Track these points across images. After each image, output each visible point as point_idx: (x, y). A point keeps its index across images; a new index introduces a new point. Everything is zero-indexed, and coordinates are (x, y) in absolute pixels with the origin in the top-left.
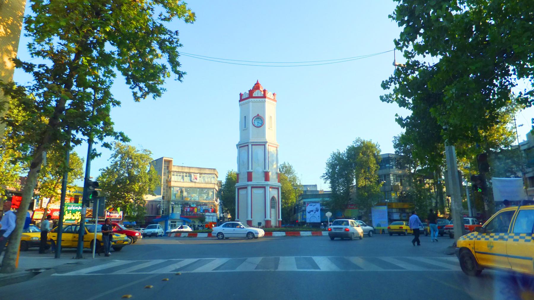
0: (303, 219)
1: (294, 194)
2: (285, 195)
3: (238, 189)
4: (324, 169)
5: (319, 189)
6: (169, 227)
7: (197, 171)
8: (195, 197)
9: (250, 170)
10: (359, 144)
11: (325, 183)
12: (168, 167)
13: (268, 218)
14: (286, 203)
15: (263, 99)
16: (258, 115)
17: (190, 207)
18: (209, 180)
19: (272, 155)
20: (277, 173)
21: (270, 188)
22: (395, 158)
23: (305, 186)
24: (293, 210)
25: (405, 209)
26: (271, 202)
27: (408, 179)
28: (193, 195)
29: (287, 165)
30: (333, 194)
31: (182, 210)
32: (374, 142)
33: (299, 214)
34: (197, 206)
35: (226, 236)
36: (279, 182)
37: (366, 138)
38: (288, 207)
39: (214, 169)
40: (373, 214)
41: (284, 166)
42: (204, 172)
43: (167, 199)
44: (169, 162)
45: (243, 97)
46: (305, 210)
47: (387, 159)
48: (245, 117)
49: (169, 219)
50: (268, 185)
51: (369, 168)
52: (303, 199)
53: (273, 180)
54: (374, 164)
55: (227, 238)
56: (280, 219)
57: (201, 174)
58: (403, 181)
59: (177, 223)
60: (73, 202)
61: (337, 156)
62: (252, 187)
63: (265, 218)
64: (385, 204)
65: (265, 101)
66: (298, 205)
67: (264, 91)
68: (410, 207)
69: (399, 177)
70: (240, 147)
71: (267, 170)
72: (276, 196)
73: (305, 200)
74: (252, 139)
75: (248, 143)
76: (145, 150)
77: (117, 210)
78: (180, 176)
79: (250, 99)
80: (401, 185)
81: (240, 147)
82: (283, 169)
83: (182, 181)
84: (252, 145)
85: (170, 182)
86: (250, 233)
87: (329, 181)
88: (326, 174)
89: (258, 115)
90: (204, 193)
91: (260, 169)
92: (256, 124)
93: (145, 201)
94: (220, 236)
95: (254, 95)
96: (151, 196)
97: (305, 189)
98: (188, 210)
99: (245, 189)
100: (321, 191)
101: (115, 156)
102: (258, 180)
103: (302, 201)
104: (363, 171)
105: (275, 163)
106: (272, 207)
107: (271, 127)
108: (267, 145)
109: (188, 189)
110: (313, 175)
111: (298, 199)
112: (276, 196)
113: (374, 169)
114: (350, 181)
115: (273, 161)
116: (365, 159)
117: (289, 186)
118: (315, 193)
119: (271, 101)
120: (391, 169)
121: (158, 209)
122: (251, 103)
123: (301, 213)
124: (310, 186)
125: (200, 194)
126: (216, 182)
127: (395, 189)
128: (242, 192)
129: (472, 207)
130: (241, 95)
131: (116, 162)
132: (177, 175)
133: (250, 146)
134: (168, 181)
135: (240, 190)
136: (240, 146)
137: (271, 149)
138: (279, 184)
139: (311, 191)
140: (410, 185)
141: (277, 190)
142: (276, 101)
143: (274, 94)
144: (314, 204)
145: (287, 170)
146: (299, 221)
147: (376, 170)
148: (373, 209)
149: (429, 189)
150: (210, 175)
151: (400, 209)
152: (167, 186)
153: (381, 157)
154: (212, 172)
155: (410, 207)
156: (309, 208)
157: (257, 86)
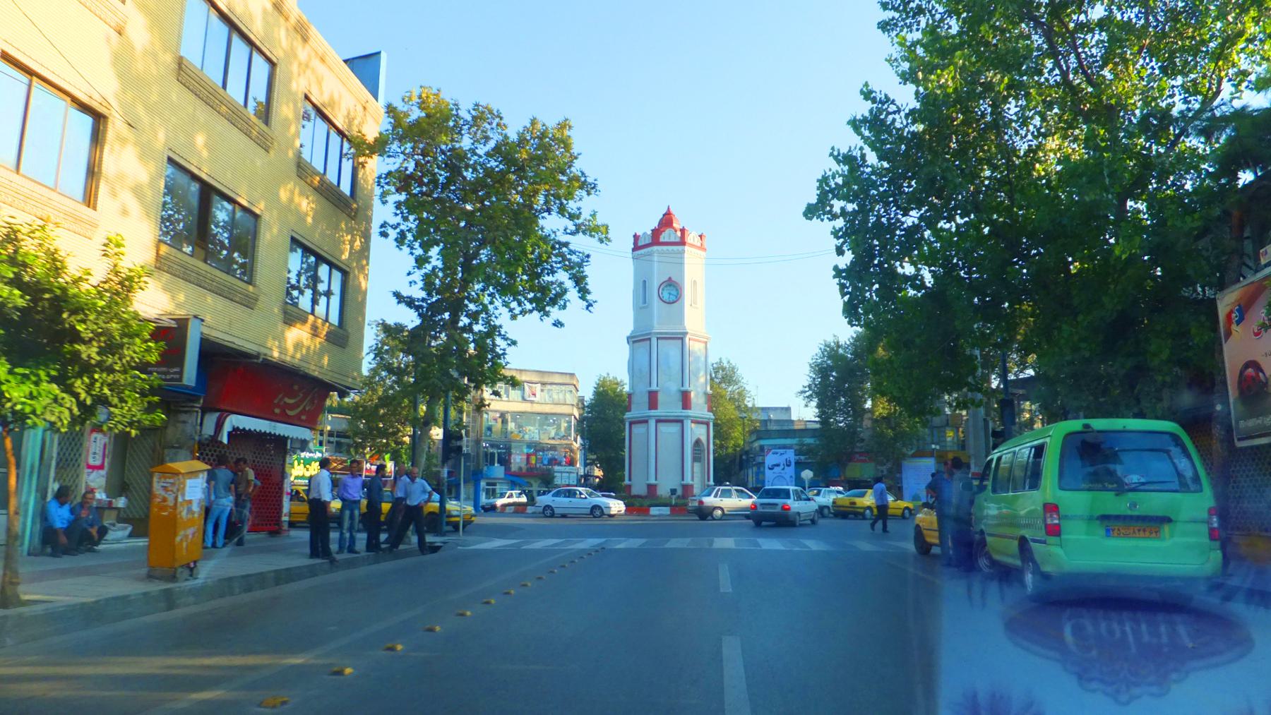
0: (757, 480)
1: (740, 428)
2: (721, 431)
3: (631, 424)
4: (803, 376)
5: (794, 417)
7: (535, 378)
9: (654, 388)
13: (688, 480)
14: (721, 447)
15: (680, 248)
18: (561, 396)
19: (698, 358)
20: (706, 394)
23: (763, 409)
29: (725, 364)
30: (825, 428)
34: (537, 451)
35: (556, 511)
38: (727, 455)
39: (572, 375)
40: (904, 476)
45: (640, 244)
50: (688, 417)
52: (759, 438)
53: (699, 407)
55: (564, 516)
57: (543, 384)
59: (498, 487)
61: (832, 349)
62: (658, 421)
64: (931, 454)
66: (747, 453)
67: (683, 231)
71: (686, 388)
72: (704, 439)
73: (762, 442)
79: (655, 248)
86: (595, 507)
87: (814, 403)
88: (809, 386)
91: (674, 387)
92: (666, 296)
94: (548, 512)
95: (662, 240)
97: (763, 417)
99: (644, 425)
103: (756, 445)
106: (696, 459)
108: (687, 339)
109: (518, 415)
111: (748, 439)
112: (704, 439)
115: (698, 370)
117: (730, 411)
123: (755, 469)
128: (638, 430)
130: (636, 237)
133: (654, 340)
136: (634, 340)
137: (694, 346)
138: (711, 415)
139: (777, 422)
141: (705, 427)
143: (701, 236)
145: (724, 376)
150: (563, 388)
154: (567, 380)
156: (770, 459)
157: (667, 221)
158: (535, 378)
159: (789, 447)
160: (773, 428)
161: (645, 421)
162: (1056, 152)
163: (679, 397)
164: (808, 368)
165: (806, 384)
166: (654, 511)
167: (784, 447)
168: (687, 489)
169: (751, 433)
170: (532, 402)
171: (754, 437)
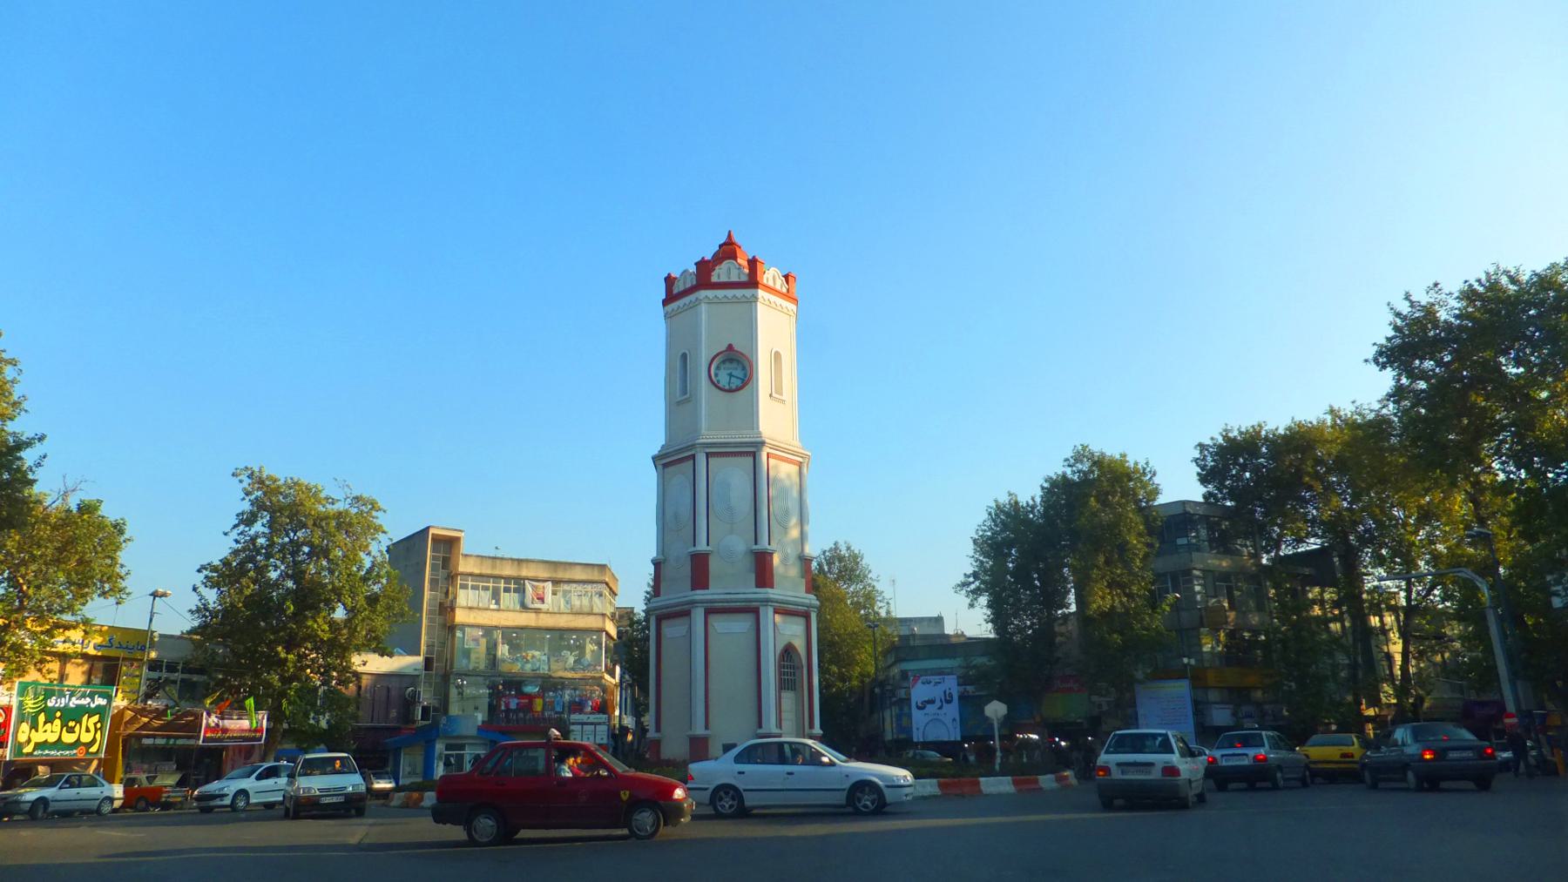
2: (833, 649)
4: (963, 560)
7: (543, 573)
8: (537, 659)
9: (702, 546)
10: (1085, 467)
11: (971, 606)
15: (748, 292)
16: (730, 347)
17: (521, 694)
18: (585, 601)
19: (784, 492)
21: (776, 612)
22: (1207, 517)
24: (867, 699)
26: (781, 667)
27: (1253, 587)
28: (530, 653)
29: (844, 552)
31: (490, 705)
32: (1135, 458)
33: (887, 714)
34: (544, 689)
36: (808, 591)
37: (1109, 446)
38: (851, 690)
39: (602, 567)
41: (834, 557)
42: (567, 575)
43: (440, 669)
44: (448, 545)
46: (909, 700)
47: (1181, 518)
48: (684, 356)
50: (767, 601)
51: (1123, 548)
52: (899, 660)
54: (1140, 535)
58: (1237, 593)
60: (95, 680)
62: (709, 612)
63: (760, 726)
64: (1180, 674)
65: (756, 298)
66: (882, 684)
67: (753, 263)
69: (1220, 581)
71: (764, 544)
72: (800, 644)
75: (693, 446)
76: (357, 499)
77: (243, 708)
78: (486, 589)
79: (703, 294)
80: (1232, 607)
81: (665, 466)
82: (830, 564)
83: (493, 606)
84: (708, 455)
85: (453, 609)
87: (983, 600)
88: (975, 575)
89: (730, 347)
90: (569, 648)
91: (739, 544)
92: (724, 380)
93: (357, 675)
95: (714, 279)
96: (376, 656)
97: (904, 631)
98: (513, 706)
99: (684, 620)
100: (957, 635)
101: (248, 520)
102: (729, 582)
103: (895, 671)
104: (1101, 559)
105: (794, 520)
106: (787, 682)
107: (779, 391)
110: (930, 582)
111: (881, 664)
112: (800, 644)
113: (1141, 550)
114: (1054, 598)
115: (787, 513)
116: (1106, 517)
118: (938, 642)
119: (779, 301)
120: (1195, 555)
121: (409, 703)
122: (704, 307)
123: (895, 710)
124: (922, 620)
126: (609, 610)
127: (1213, 620)
129: (1514, 676)
130: (669, 281)
131: (253, 539)
132: (474, 588)
134: (446, 608)
135: (664, 624)
136: (665, 461)
138: (812, 599)
140: (1260, 608)
141: (802, 621)
142: (795, 301)
143: (786, 277)
144: (937, 678)
145: (845, 566)
146: (888, 737)
147: (1146, 556)
149: (1324, 621)
150: (589, 587)
152: (444, 626)
156: (919, 692)
157: (728, 250)
158: (543, 573)
160: (925, 645)
161: (683, 613)
164: (972, 546)
165: (970, 571)
167: (940, 672)
169: (885, 653)
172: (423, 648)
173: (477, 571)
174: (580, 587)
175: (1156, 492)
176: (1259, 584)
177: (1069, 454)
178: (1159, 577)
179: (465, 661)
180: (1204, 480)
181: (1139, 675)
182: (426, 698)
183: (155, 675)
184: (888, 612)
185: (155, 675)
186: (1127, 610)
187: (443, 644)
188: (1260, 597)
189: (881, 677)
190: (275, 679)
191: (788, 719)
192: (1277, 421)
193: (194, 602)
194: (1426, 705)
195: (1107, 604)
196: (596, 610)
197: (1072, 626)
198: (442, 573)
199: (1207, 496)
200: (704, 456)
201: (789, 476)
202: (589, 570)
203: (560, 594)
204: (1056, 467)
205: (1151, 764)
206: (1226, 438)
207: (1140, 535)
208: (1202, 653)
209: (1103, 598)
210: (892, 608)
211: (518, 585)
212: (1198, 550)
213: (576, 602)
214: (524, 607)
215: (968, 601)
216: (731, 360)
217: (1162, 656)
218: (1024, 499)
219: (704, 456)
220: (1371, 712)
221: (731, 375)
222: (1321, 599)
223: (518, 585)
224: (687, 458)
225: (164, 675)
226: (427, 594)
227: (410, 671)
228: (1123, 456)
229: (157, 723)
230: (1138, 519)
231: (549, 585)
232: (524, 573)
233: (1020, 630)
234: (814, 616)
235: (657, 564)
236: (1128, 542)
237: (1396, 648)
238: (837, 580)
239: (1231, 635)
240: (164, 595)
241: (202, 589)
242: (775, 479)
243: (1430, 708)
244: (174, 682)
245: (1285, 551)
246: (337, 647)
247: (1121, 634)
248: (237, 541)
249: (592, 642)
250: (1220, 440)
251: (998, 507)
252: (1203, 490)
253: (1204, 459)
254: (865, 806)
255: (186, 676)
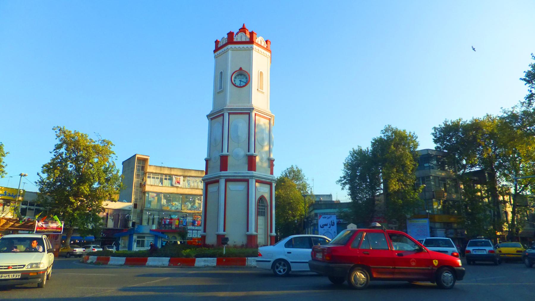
4: (340, 172)
6: (135, 245)
7: (180, 173)
8: (176, 205)
9: (225, 152)
10: (389, 134)
11: (343, 189)
12: (143, 168)
13: (252, 231)
15: (249, 46)
16: (241, 69)
19: (262, 130)
21: (257, 181)
23: (317, 196)
25: (451, 223)
28: (174, 203)
29: (295, 169)
42: (189, 174)
44: (144, 161)
47: (426, 157)
48: (221, 73)
49: (134, 233)
50: (252, 177)
51: (404, 166)
52: (314, 209)
56: (274, 234)
58: (448, 186)
59: (146, 239)
62: (227, 181)
63: (248, 231)
64: (426, 216)
65: (252, 48)
66: (307, 218)
67: (252, 34)
68: (459, 220)
70: (212, 119)
71: (252, 152)
72: (267, 196)
73: (316, 211)
74: (230, 103)
76: (104, 141)
78: (158, 178)
79: (230, 46)
81: (212, 119)
84: (229, 114)
85: (145, 185)
87: (347, 186)
88: (344, 177)
89: (241, 69)
91: (242, 152)
92: (238, 83)
95: (235, 40)
97: (317, 199)
101: (59, 147)
104: (395, 170)
105: (266, 143)
106: (260, 212)
107: (262, 88)
110: (327, 181)
111: (307, 211)
112: (267, 196)
114: (373, 187)
115: (263, 140)
119: (263, 51)
120: (432, 170)
121: (126, 220)
122: (230, 52)
123: (312, 228)
125: (183, 202)
130: (217, 42)
132: (153, 178)
133: (226, 115)
134: (142, 185)
136: (213, 117)
140: (457, 192)
141: (268, 186)
142: (270, 51)
143: (267, 41)
144: (329, 216)
145: (295, 174)
148: (409, 222)
149: (482, 198)
150: (197, 179)
151: (444, 223)
153: (420, 154)
155: (459, 220)
156: (322, 221)
158: (180, 173)
159: (334, 214)
160: (326, 204)
162: (387, 164)
163: (245, 160)
164: (343, 166)
165: (342, 176)
166: (200, 262)
168: (251, 239)
169: (309, 207)
170: (177, 187)
171: (311, 209)
172: (133, 199)
173: (154, 172)
174: (193, 179)
175: (416, 145)
176: (456, 182)
177: (383, 128)
178: (417, 179)
179: (149, 205)
180: (436, 141)
181: (408, 216)
182: (133, 218)
183: (24, 207)
184: (311, 192)
185: (24, 207)
186: (405, 190)
187: (141, 198)
188: (457, 187)
189: (307, 215)
190: (69, 210)
191: (260, 228)
192: (467, 118)
193: (38, 178)
194: (520, 232)
195: (397, 188)
196: (199, 188)
197: (382, 197)
198: (141, 172)
199: (437, 148)
200: (228, 115)
201: (265, 124)
202: (197, 172)
203: (186, 181)
204: (378, 134)
205: (447, 252)
206: (446, 125)
207: (411, 161)
208: (433, 208)
209: (395, 185)
210: (313, 191)
211: (170, 177)
212: (433, 168)
213: (192, 184)
214: (172, 185)
215: (341, 187)
216: (241, 75)
217: (419, 210)
218: (364, 148)
219: (228, 115)
220: (498, 234)
221: (241, 81)
222: (481, 190)
223: (170, 177)
224: (220, 116)
225: (28, 207)
226: (135, 180)
227: (127, 208)
228: (404, 131)
229: (17, 225)
230: (409, 154)
231: (182, 178)
232: (173, 173)
233: (361, 199)
234: (274, 185)
235: (207, 161)
236: (406, 163)
237: (509, 209)
238: (292, 179)
239: (444, 202)
240: (25, 175)
241: (41, 174)
242: (258, 125)
243: (521, 233)
244: (33, 210)
245: (467, 171)
246: (95, 196)
247: (402, 200)
248: (55, 155)
249: (198, 199)
250: (443, 126)
251: (354, 151)
252: (435, 145)
253: (436, 133)
254: (280, 272)
255: (30, 207)
